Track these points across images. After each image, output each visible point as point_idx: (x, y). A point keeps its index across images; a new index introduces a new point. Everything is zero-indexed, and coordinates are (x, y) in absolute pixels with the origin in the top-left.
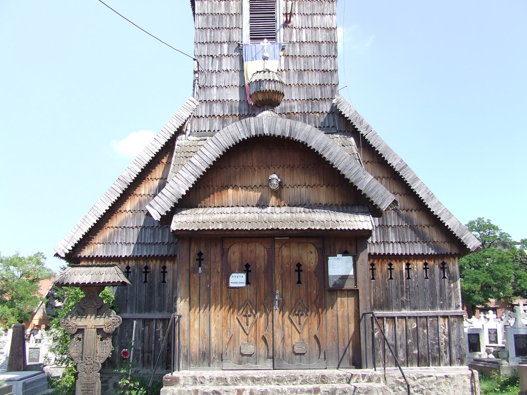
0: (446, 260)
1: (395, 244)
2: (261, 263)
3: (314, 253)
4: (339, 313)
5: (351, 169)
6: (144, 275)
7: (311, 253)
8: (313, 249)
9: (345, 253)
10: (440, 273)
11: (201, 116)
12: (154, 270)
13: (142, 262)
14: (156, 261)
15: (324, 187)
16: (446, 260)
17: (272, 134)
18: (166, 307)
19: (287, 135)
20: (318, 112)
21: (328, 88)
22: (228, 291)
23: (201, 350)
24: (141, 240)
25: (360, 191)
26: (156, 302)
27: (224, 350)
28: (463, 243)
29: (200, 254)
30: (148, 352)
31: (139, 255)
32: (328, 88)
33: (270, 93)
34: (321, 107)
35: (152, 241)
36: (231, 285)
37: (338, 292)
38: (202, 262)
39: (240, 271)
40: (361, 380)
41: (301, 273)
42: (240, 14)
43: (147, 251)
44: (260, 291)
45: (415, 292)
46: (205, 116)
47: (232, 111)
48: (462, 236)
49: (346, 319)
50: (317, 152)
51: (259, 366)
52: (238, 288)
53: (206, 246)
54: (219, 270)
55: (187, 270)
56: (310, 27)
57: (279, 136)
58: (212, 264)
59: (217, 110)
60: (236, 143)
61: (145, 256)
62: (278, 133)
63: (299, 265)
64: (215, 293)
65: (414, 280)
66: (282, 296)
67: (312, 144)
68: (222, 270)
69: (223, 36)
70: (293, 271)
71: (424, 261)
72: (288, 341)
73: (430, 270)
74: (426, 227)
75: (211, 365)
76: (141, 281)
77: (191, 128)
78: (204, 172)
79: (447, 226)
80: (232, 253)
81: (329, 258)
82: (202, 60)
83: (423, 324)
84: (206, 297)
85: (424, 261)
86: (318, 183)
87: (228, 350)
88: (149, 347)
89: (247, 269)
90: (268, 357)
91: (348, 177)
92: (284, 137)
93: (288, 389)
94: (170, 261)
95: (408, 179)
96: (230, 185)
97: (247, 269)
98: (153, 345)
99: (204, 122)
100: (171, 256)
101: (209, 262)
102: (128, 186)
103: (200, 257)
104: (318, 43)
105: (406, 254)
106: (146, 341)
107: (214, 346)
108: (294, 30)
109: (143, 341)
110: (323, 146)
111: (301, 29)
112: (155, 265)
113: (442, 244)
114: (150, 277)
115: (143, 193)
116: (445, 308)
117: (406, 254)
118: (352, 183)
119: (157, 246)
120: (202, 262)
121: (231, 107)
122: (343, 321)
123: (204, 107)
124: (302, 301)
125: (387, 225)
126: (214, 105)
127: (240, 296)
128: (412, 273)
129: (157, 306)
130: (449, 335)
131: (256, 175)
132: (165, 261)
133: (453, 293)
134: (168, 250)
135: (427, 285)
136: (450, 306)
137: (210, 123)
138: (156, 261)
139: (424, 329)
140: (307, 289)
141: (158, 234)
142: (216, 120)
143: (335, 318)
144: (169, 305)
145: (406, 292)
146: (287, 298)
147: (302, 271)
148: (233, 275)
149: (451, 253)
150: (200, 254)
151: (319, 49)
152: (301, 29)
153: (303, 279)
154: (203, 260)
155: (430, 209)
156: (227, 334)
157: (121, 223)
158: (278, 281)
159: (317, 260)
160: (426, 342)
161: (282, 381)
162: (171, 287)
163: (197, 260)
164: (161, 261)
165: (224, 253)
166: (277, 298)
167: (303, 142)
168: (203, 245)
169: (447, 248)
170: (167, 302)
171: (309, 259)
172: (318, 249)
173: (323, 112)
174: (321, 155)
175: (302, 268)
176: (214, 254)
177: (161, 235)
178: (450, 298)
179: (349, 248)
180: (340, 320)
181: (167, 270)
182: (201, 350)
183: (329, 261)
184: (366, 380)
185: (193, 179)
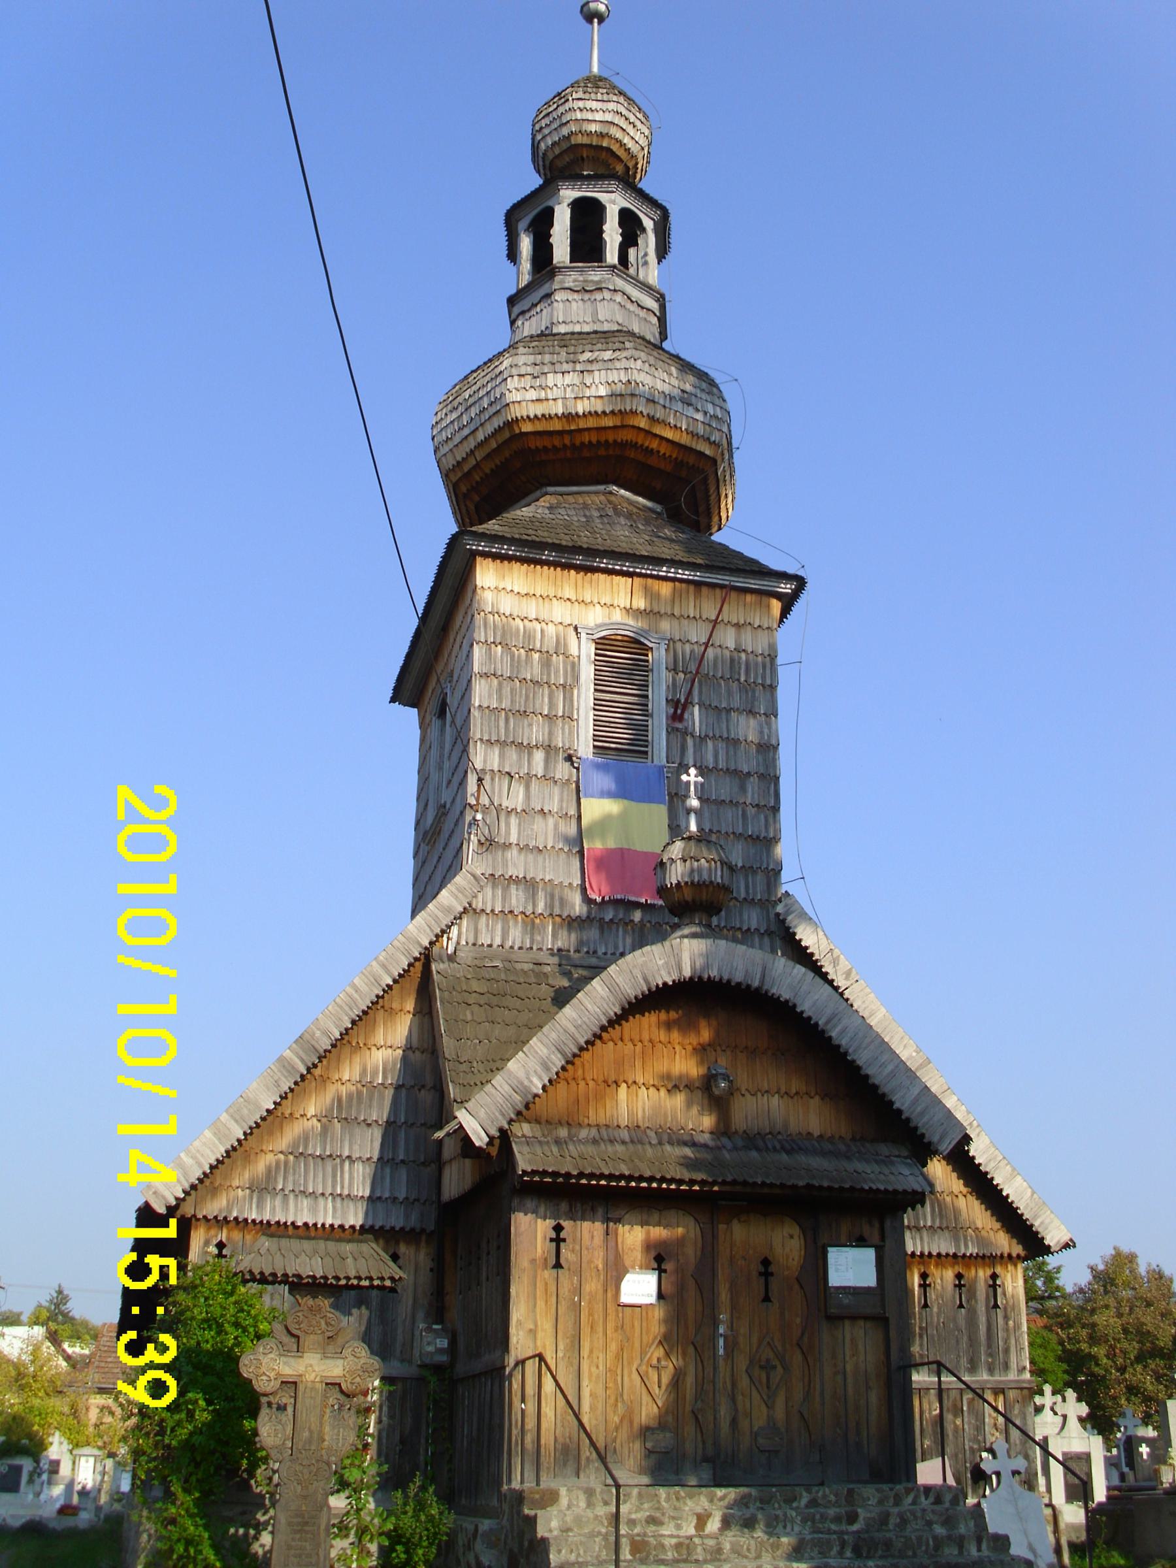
3: (796, 1237)
4: (849, 1368)
7: (791, 1237)
8: (796, 1231)
9: (861, 1242)
11: (483, 910)
17: (726, 978)
18: (398, 1351)
19: (756, 984)
20: (740, 929)
21: (760, 877)
22: (617, 1311)
23: (560, 1440)
24: (342, 1187)
25: (899, 1112)
27: (609, 1440)
28: (1037, 1233)
31: (337, 1223)
32: (760, 877)
33: (711, 889)
34: (745, 917)
36: (625, 1299)
38: (562, 1244)
40: (923, 1499)
41: (771, 1279)
45: (939, 1336)
46: (492, 911)
47: (552, 907)
50: (816, 1024)
53: (571, 1210)
54: (600, 1266)
56: (725, 735)
57: (739, 984)
58: (585, 1252)
59: (517, 899)
62: (738, 977)
63: (766, 1262)
64: (591, 1314)
65: (935, 1310)
66: (731, 1327)
67: (806, 1006)
69: (536, 732)
70: (755, 1274)
72: (744, 1424)
73: (968, 1291)
74: (960, 1196)
75: (582, 1475)
79: (1008, 1196)
81: (830, 1249)
83: (955, 1406)
84: (570, 1324)
86: (804, 1089)
87: (618, 1441)
90: (706, 1459)
91: (876, 1082)
92: (749, 986)
94: (408, 1243)
96: (621, 1079)
99: (488, 925)
100: (413, 1230)
101: (578, 1247)
103: (558, 1235)
108: (690, 741)
110: (829, 1012)
111: (703, 739)
113: (991, 1233)
115: (346, 1077)
116: (997, 1371)
118: (884, 1095)
120: (562, 1244)
121: (552, 896)
123: (489, 891)
124: (772, 1339)
126: (513, 887)
127: (644, 1324)
128: (932, 1295)
132: (397, 1243)
134: (407, 1216)
135: (962, 1323)
136: (1006, 1367)
137: (503, 929)
139: (955, 1416)
142: (516, 922)
143: (839, 1378)
145: (921, 1336)
146: (742, 1331)
147: (772, 1274)
154: (564, 1240)
155: (974, 1158)
156: (616, 1405)
157: (296, 1144)
158: (724, 1296)
160: (961, 1446)
161: (768, 1502)
162: (410, 1302)
163: (552, 1240)
166: (721, 1331)
167: (787, 1001)
169: (1003, 1242)
170: (400, 1338)
172: (804, 1231)
173: (749, 929)
174: (823, 1031)
175: (772, 1269)
177: (388, 1180)
178: (1007, 1351)
179: (867, 1230)
180: (850, 1381)
182: (560, 1440)
183: (829, 1255)
184: (931, 1499)
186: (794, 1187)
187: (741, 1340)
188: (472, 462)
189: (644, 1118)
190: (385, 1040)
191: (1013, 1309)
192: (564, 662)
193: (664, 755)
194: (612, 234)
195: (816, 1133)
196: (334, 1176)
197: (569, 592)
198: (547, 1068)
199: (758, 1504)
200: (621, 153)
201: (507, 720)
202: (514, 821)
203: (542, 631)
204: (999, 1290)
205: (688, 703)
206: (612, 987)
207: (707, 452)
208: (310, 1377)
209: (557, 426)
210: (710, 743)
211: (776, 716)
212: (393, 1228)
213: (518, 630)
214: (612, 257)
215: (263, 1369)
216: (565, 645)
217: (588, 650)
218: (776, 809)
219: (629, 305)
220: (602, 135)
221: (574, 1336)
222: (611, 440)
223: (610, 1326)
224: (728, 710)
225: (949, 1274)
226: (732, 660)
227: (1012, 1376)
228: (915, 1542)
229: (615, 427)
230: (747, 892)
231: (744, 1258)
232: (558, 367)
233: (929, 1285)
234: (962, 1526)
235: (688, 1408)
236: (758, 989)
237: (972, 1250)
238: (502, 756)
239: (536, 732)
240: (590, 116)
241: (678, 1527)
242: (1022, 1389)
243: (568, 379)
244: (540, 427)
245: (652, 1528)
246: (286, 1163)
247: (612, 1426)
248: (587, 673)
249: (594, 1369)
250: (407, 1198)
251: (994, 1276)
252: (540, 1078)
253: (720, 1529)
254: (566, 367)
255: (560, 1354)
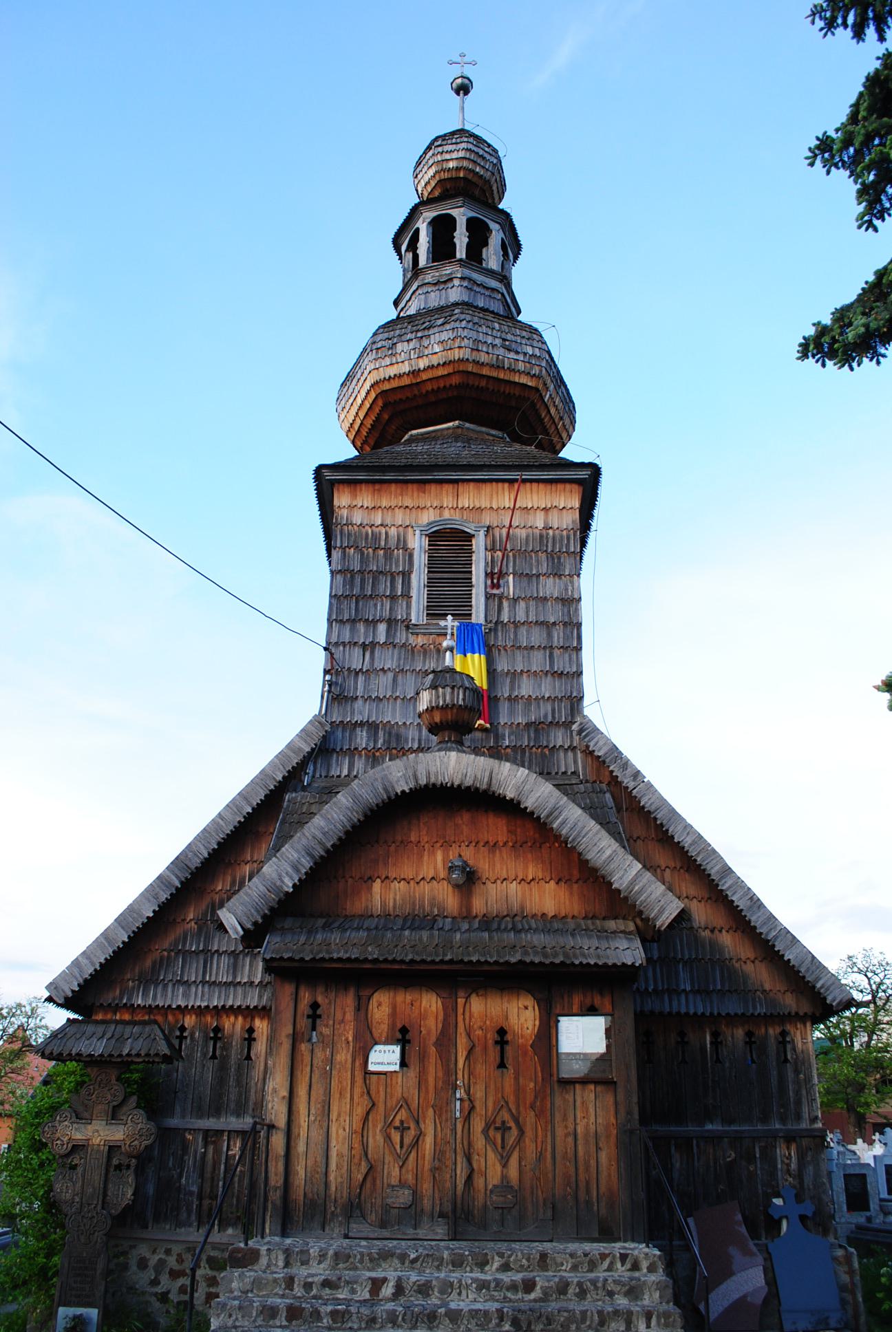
0: (788, 1027)
1: (691, 996)
2: (432, 1026)
3: (530, 1008)
4: (579, 1130)
5: (601, 851)
6: (212, 1043)
7: (526, 1008)
9: (592, 1011)
10: (778, 1053)
12: (232, 1036)
13: (209, 1019)
14: (236, 1018)
15: (552, 883)
16: (788, 1027)
19: (484, 787)
26: (232, 1097)
29: (315, 1006)
30: (211, 1198)
31: (204, 1004)
35: (230, 979)
36: (371, 1068)
37: (577, 1086)
39: (388, 1042)
40: (619, 1265)
42: (406, 575)
43: (219, 997)
44: (426, 1081)
48: (818, 979)
49: (592, 1141)
51: (421, 1233)
52: (385, 1073)
54: (350, 1039)
55: (288, 1036)
57: (469, 788)
58: (337, 1026)
60: (389, 798)
61: (216, 1007)
63: (502, 1032)
65: (727, 1065)
68: (355, 1038)
70: (490, 1042)
71: (746, 1027)
72: (479, 1182)
75: (327, 1228)
76: (204, 1055)
77: (314, 771)
78: (327, 851)
80: (375, 1004)
81: (561, 1019)
82: (338, 652)
84: (321, 1091)
85: (746, 1027)
88: (212, 1187)
89: (403, 1037)
90: (441, 1215)
92: (477, 789)
93: (474, 1280)
94: (262, 1018)
95: (713, 872)
97: (404, 1036)
98: (221, 1183)
101: (331, 1022)
102: (192, 874)
104: (548, 626)
105: (711, 1014)
106: (208, 1175)
107: (333, 1189)
108: (505, 604)
109: (202, 1176)
110: (550, 806)
111: (515, 600)
112: (234, 1025)
113: (780, 995)
114: (223, 1048)
117: (711, 1014)
119: (240, 990)
120: (318, 1021)
121: (390, 733)
122: (587, 1142)
125: (674, 958)
126: (358, 730)
129: (232, 1106)
130: (800, 1176)
131: (426, 858)
132: (253, 1019)
133: (804, 1092)
134: (260, 997)
136: (799, 1117)
138: (236, 1018)
140: (517, 1078)
141: (243, 966)
142: (360, 756)
143: (570, 1139)
144: (255, 1104)
147: (507, 1042)
148: (377, 1047)
149: (797, 1013)
150: (315, 1006)
151: (550, 635)
152: (515, 600)
153: (510, 1060)
154: (320, 1016)
159: (537, 1023)
161: (461, 1265)
163: (309, 1017)
164: (245, 1018)
165: (361, 1007)
167: (512, 800)
168: (320, 989)
169: (790, 1002)
171: (522, 1020)
175: (509, 1037)
176: (341, 1006)
178: (798, 1103)
179: (597, 1001)
180: (580, 1141)
181: (255, 1035)
182: (310, 1195)
184: (628, 1266)
185: (307, 864)
186: (507, 963)
187: (478, 1104)
188: (358, 422)
189: (394, 907)
190: (252, 857)
191: (803, 1063)
192: (404, 556)
193: (482, 615)
194: (461, 239)
195: (551, 914)
196: (205, 967)
197: (408, 502)
198: (297, 870)
199: (450, 1267)
200: (475, 180)
201: (357, 603)
202: (361, 678)
203: (386, 533)
204: (789, 1047)
205: (502, 575)
206: (355, 798)
207: (530, 384)
208: (96, 1141)
209: (406, 381)
210: (522, 604)
211: (579, 575)
212: (248, 1007)
213: (367, 534)
214: (461, 253)
215: (58, 1135)
216: (405, 542)
217: (418, 543)
218: (578, 649)
219: (475, 288)
220: (458, 169)
221: (324, 1101)
222: (491, 388)
223: (357, 1091)
224: (538, 576)
225: (740, 1033)
226: (541, 536)
227: (804, 1125)
228: (578, 1316)
229: (449, 374)
230: (553, 717)
231: (481, 1028)
232: (403, 338)
233: (721, 1043)
234: (646, 1297)
235: (427, 1167)
236: (485, 791)
237: (761, 1010)
238: (353, 630)
239: (382, 608)
240: (448, 156)
241: (353, 1291)
242: (814, 1137)
243: (412, 345)
244: (395, 384)
245: (327, 1291)
246: (169, 957)
247: (356, 1184)
248: (420, 561)
249: (341, 1131)
250: (261, 982)
251: (784, 1034)
252: (291, 878)
253: (393, 1294)
254: (409, 336)
255: (312, 1118)
